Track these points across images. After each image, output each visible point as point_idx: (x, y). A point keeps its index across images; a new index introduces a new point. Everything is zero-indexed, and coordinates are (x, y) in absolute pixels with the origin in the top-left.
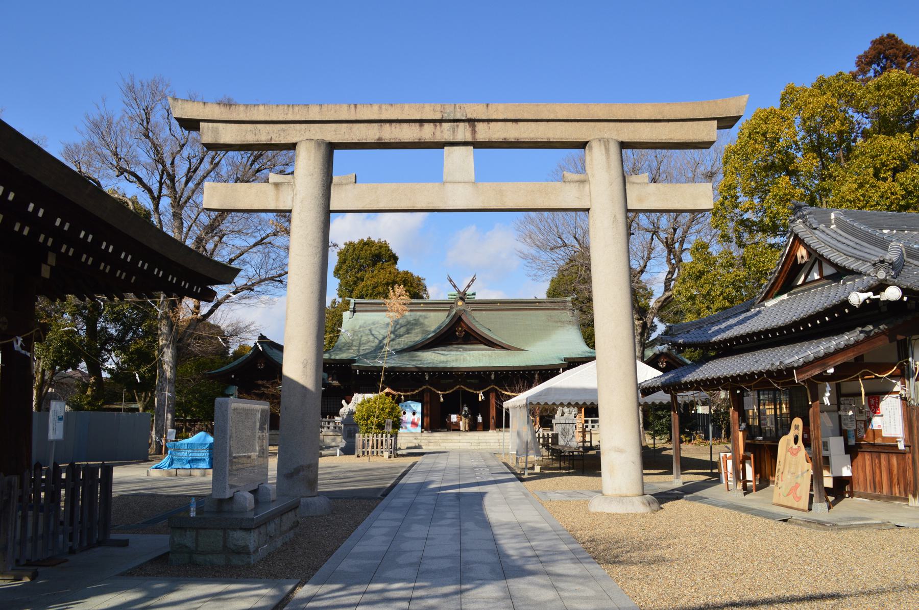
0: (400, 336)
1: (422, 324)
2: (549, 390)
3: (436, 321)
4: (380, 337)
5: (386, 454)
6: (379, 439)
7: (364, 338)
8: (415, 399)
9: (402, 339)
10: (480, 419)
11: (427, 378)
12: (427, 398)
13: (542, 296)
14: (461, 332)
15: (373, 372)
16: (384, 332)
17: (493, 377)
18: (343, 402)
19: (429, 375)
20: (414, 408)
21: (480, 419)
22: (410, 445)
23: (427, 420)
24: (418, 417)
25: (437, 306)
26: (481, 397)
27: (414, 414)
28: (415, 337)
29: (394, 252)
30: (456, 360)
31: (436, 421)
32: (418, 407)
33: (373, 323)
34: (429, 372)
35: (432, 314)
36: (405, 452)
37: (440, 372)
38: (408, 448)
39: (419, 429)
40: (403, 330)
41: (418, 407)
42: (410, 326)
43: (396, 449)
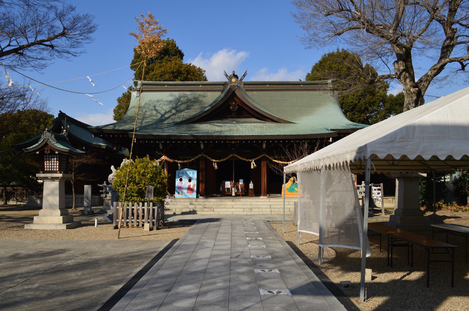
0: (181, 111)
1: (201, 101)
2: (409, 131)
3: (211, 98)
4: (163, 112)
5: (147, 226)
6: (146, 208)
7: (148, 113)
8: (191, 166)
9: (183, 114)
10: (251, 186)
11: (202, 147)
12: (202, 166)
13: (303, 80)
14: (234, 106)
15: (149, 140)
16: (167, 108)
17: (264, 146)
18: (112, 168)
19: (204, 144)
20: (191, 175)
21: (251, 186)
22: (184, 210)
23: (202, 186)
24: (193, 184)
25: (214, 86)
26: (253, 165)
27: (190, 180)
28: (194, 111)
29: (180, 48)
30: (230, 131)
31: (210, 187)
32: (193, 174)
33: (158, 101)
34: (204, 141)
35: (209, 94)
36: (175, 219)
37: (214, 141)
38: (183, 214)
39: (194, 195)
40: (183, 107)
41: (193, 174)
42: (189, 104)
43: (164, 217)
